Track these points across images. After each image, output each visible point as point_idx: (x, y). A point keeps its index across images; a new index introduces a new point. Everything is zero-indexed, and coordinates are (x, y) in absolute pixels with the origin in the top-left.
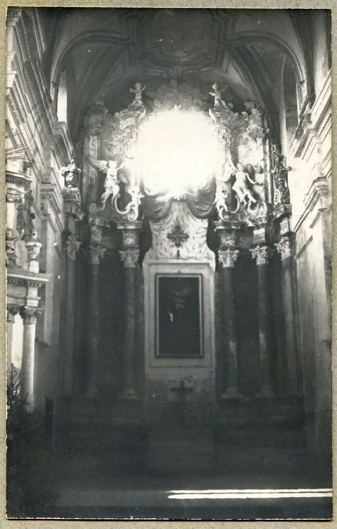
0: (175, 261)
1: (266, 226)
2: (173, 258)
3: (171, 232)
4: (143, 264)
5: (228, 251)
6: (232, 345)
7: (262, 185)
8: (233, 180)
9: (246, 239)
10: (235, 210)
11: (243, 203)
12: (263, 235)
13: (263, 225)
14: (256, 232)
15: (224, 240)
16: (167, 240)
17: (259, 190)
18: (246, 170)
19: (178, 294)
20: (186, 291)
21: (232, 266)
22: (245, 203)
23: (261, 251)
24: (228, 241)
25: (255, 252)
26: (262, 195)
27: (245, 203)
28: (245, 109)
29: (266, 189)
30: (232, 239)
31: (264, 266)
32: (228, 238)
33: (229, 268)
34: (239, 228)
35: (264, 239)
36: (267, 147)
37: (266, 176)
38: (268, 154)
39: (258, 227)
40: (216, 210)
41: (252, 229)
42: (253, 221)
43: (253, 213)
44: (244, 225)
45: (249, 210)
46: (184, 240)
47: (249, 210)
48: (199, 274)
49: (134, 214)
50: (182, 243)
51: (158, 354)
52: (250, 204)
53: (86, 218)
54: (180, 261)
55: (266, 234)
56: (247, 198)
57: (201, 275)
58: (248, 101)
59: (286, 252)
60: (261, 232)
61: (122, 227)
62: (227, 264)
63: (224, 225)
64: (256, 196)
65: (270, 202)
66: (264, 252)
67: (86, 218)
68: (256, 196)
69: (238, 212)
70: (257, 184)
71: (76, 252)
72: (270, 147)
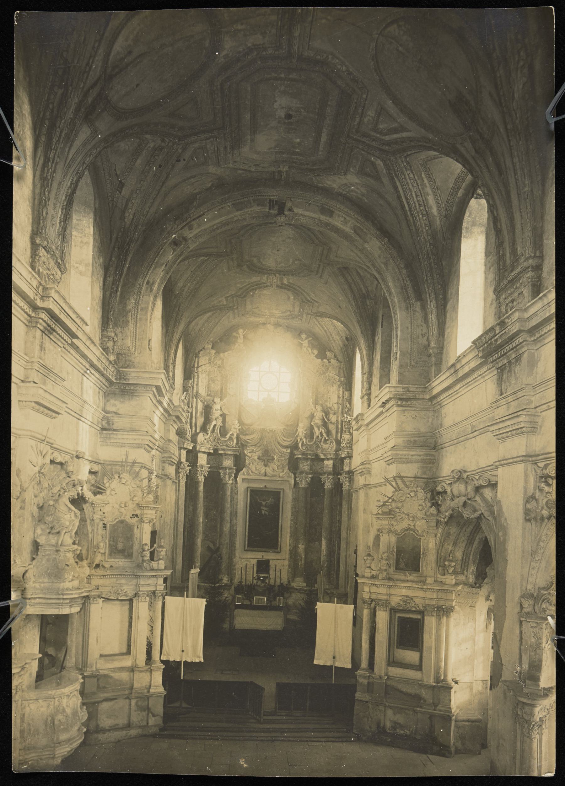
0: (264, 478)
1: (335, 460)
2: (261, 475)
3: (261, 455)
4: (238, 479)
5: (304, 475)
6: (301, 547)
7: (334, 424)
8: (312, 417)
9: (261, 557)
10: (312, 441)
11: (318, 437)
12: (331, 466)
13: (331, 459)
14: (326, 462)
15: (301, 465)
16: (258, 460)
17: (332, 427)
18: (323, 411)
19: (264, 503)
20: (270, 501)
21: (306, 486)
22: (320, 437)
23: (328, 478)
24: (304, 466)
25: (323, 478)
26: (334, 432)
27: (320, 437)
28: (326, 358)
29: (337, 427)
30: (307, 465)
31: (331, 490)
32: (305, 464)
33: (303, 489)
34: (313, 457)
35: (332, 469)
36: (341, 392)
37: (338, 417)
38: (341, 399)
39: (328, 459)
40: (297, 441)
41: (323, 460)
42: (324, 455)
43: (326, 446)
44: (317, 456)
45: (322, 444)
46: (271, 461)
47: (322, 444)
48: (280, 489)
49: (233, 441)
50: (269, 464)
51: (246, 548)
52: (323, 439)
53: (194, 447)
54: (267, 478)
55: (334, 465)
56: (321, 434)
57: (283, 490)
58: (329, 351)
59: (346, 486)
60: (329, 464)
61: (222, 452)
62: (303, 485)
63: (302, 455)
64: (328, 433)
65: (339, 438)
66: (330, 480)
67: (194, 447)
68: (328, 433)
69: (315, 443)
70: (331, 423)
71: (187, 475)
72: (343, 392)
